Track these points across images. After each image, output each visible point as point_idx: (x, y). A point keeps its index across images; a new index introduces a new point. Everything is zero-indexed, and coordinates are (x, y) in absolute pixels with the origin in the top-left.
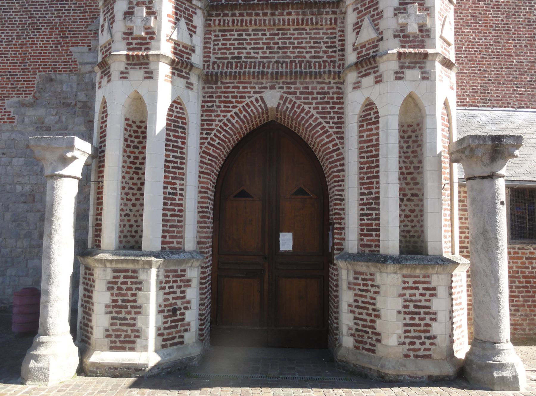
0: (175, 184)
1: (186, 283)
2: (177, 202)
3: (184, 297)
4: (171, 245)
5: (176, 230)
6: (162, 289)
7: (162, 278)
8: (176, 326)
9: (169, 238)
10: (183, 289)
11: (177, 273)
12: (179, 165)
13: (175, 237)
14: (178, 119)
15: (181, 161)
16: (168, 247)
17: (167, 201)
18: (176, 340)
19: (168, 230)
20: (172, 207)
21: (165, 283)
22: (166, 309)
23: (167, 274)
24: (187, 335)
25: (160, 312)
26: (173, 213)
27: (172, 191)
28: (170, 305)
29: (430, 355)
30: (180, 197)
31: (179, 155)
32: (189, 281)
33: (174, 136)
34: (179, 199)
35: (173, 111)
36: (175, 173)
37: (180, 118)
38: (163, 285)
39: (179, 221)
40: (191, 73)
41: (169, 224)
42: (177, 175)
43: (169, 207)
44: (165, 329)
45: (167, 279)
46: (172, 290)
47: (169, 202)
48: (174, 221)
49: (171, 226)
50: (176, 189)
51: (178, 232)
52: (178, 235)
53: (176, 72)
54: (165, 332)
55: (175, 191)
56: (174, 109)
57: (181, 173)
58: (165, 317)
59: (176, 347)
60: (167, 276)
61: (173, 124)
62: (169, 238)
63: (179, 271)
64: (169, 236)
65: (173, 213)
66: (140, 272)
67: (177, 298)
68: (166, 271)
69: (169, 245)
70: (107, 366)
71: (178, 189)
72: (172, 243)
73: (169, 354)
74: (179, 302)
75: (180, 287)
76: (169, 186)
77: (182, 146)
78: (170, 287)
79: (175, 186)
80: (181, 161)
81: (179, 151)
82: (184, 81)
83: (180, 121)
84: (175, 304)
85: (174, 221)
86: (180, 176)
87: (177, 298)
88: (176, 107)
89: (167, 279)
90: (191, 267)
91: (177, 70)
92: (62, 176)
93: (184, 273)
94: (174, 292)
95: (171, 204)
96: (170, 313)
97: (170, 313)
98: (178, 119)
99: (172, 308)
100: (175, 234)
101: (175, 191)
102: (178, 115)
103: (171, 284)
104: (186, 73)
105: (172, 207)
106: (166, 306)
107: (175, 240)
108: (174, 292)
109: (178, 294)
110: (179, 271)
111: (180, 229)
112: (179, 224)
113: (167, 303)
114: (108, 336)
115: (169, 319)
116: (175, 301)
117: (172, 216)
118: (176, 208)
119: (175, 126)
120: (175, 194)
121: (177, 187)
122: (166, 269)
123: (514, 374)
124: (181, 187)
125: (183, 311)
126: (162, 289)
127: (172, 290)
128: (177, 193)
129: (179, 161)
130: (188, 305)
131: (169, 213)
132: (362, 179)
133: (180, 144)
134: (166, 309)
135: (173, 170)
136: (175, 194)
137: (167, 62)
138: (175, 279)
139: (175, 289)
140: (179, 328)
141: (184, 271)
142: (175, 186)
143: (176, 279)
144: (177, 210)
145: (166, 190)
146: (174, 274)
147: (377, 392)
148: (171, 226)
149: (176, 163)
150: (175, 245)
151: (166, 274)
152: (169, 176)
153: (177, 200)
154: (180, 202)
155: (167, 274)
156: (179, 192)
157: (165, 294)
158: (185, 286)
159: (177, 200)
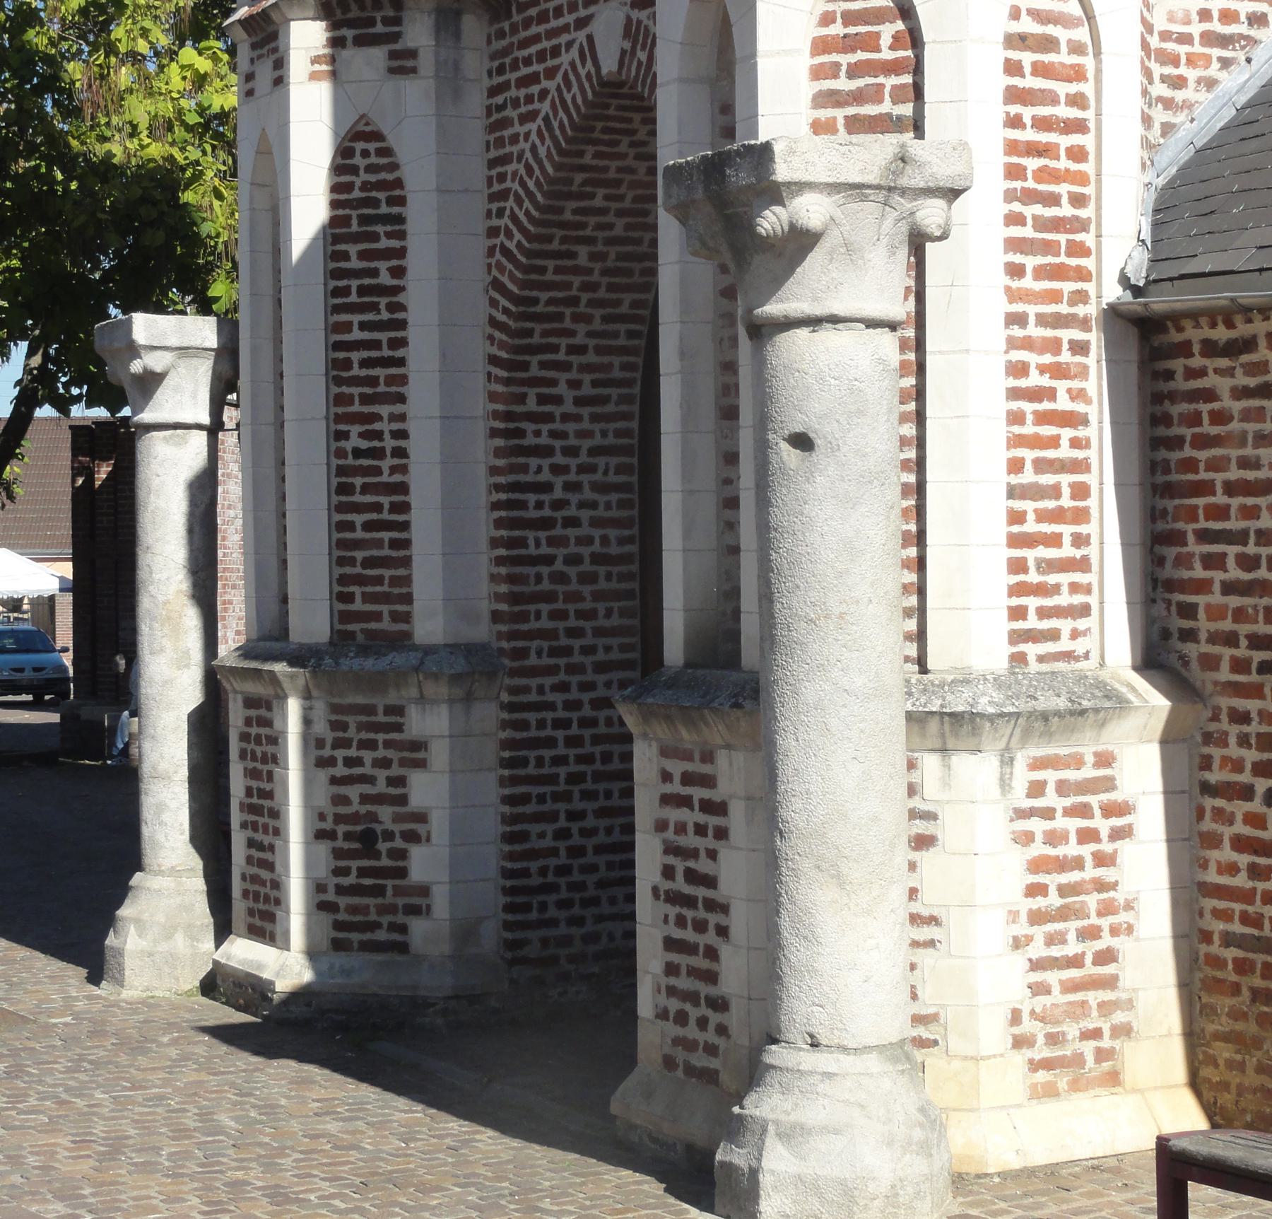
0: (377, 417)
1: (406, 754)
2: (385, 478)
3: (403, 800)
4: (373, 626)
5: (387, 573)
6: (323, 763)
7: (321, 728)
8: (379, 891)
9: (364, 602)
10: (396, 771)
11: (373, 719)
12: (386, 352)
13: (386, 598)
14: (374, 194)
15: (393, 334)
16: (362, 631)
17: (350, 480)
18: (381, 935)
19: (359, 575)
20: (369, 499)
21: (334, 747)
22: (341, 829)
23: (340, 717)
24: (418, 928)
25: (320, 835)
26: (374, 516)
27: (364, 444)
28: (355, 818)
29: (716, 1072)
30: (396, 461)
31: (385, 315)
32: (418, 745)
33: (363, 255)
34: (393, 470)
35: (354, 170)
36: (373, 381)
37: (382, 185)
38: (327, 752)
39: (395, 544)
40: (406, 15)
41: (359, 555)
42: (382, 388)
43: (358, 498)
44: (340, 890)
45: (340, 734)
46: (357, 771)
47: (358, 481)
48: (379, 544)
49: (369, 563)
50: (378, 435)
51: (395, 581)
52: (396, 591)
53: (349, 33)
54: (343, 901)
55: (376, 444)
56: (358, 160)
57: (394, 376)
58: (338, 854)
59: (379, 957)
60: (336, 726)
61: (354, 213)
62: (364, 602)
63: (381, 710)
64: (363, 594)
65: (374, 516)
66: (413, 713)
67: (379, 799)
68: (335, 709)
69: (365, 626)
70: (233, 976)
71: (387, 436)
72: (377, 616)
73: (346, 972)
74: (385, 813)
75: (385, 763)
76: (355, 429)
77: (395, 282)
78: (349, 762)
79: (377, 426)
80: (393, 334)
81: (383, 301)
82: (378, 54)
83: (382, 196)
84: (373, 817)
85: (379, 544)
86: (393, 389)
87: (379, 799)
88: (365, 154)
89: (340, 734)
90: (422, 700)
91: (351, 24)
92: (790, 324)
93: (399, 719)
94: (370, 780)
95: (366, 489)
96: (355, 845)
97: (355, 845)
98: (374, 194)
99: (359, 828)
100: (385, 588)
101: (376, 444)
102: (372, 178)
103: (353, 752)
104: (387, 21)
105: (369, 499)
106: (339, 819)
107: (385, 609)
108: (370, 780)
109: (381, 787)
110: (381, 710)
111: (401, 572)
112: (394, 554)
113: (342, 810)
114: (1020, 1042)
115: (354, 864)
116: (369, 807)
117: (368, 526)
118: (385, 500)
119: (364, 220)
120: (378, 453)
121: (384, 426)
122: (336, 700)
123: (754, 1164)
124: (395, 426)
125: (399, 843)
126: (323, 763)
127: (357, 771)
128: (383, 449)
129: (383, 336)
130: (420, 828)
132: (1019, 369)
133: (385, 279)
134: (341, 829)
135: (364, 372)
136: (378, 453)
137: (311, 14)
138: (365, 735)
139: (367, 769)
140: (389, 898)
141: (399, 710)
142: (377, 426)
143: (372, 736)
144: (387, 506)
145: (342, 444)
146: (364, 718)
147: (307, 1082)
148: (369, 563)
149: (376, 345)
150: (386, 625)
151: (334, 717)
152: (351, 396)
153: (386, 472)
154: (397, 478)
155: (340, 717)
156: (389, 443)
157: (334, 781)
158: (403, 763)
159: (386, 472)
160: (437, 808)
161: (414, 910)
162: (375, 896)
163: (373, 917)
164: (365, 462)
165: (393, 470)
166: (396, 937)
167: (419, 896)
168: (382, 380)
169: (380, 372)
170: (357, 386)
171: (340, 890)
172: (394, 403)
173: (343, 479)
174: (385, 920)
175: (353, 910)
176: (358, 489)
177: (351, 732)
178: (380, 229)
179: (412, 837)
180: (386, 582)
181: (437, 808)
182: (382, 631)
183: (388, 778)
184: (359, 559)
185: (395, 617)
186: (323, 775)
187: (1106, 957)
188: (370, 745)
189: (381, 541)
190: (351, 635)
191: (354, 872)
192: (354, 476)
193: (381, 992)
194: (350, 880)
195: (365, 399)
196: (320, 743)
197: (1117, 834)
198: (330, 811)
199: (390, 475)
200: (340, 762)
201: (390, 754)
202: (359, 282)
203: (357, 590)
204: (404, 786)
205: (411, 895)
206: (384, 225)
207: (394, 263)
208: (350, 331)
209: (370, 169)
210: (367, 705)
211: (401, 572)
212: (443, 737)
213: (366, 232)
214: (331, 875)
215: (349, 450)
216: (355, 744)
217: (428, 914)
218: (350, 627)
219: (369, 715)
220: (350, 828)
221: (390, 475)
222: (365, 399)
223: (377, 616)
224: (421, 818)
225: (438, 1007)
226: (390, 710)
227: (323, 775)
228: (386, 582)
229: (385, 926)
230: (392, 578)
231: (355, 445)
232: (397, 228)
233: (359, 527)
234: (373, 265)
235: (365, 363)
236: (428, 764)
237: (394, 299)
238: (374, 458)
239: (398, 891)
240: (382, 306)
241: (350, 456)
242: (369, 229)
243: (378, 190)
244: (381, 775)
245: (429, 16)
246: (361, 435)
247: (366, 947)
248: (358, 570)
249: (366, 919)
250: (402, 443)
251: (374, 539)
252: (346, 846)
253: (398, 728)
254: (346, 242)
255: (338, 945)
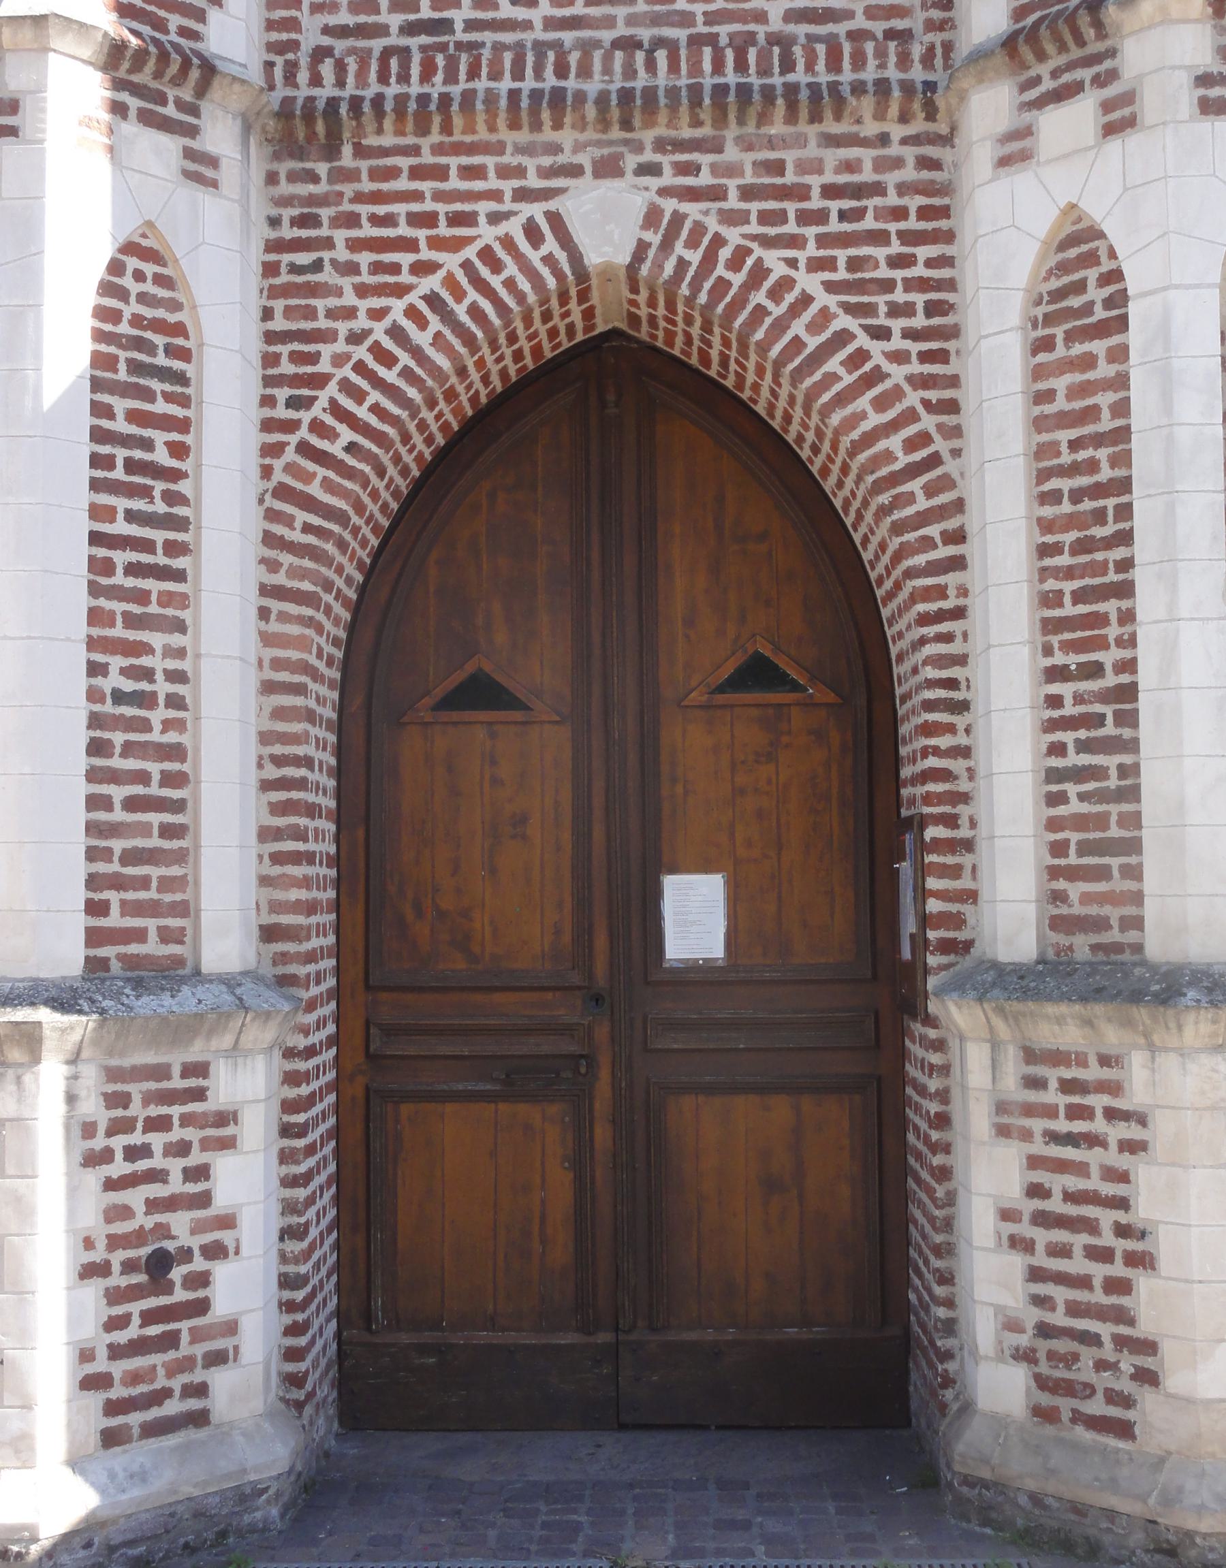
0: (147, 649)
2: (155, 736)
4: (134, 949)
5: (154, 872)
7: (92, 1107)
8: (171, 1340)
10: (196, 1158)
11: (165, 1085)
12: (161, 559)
14: (148, 335)
16: (121, 958)
17: (106, 735)
18: (172, 1407)
19: (117, 875)
20: (132, 764)
21: (110, 1133)
23: (119, 1087)
24: (221, 1381)
26: (138, 790)
27: (128, 686)
28: (139, 1237)
30: (172, 714)
31: (160, 507)
33: (134, 416)
34: (167, 725)
35: (122, 294)
36: (142, 597)
38: (99, 1143)
39: (168, 831)
41: (118, 845)
42: (154, 609)
43: (117, 762)
45: (119, 1113)
46: (142, 1165)
47: (118, 738)
48: (145, 830)
49: (130, 857)
50: (147, 674)
51: (167, 884)
52: (168, 898)
53: (134, 103)
54: (119, 1368)
55: (144, 686)
56: (127, 281)
57: (170, 594)
58: (115, 1296)
60: (117, 1100)
61: (123, 355)
63: (176, 1071)
64: (123, 903)
65: (138, 790)
67: (171, 1204)
68: (114, 1075)
69: (122, 949)
71: (159, 676)
72: (139, 935)
73: (141, 1476)
74: (180, 1222)
75: (182, 1149)
76: (116, 662)
78: (132, 1153)
79: (145, 661)
81: (159, 487)
83: (159, 340)
84: (163, 1231)
85: (145, 830)
86: (170, 612)
87: (171, 1204)
88: (139, 276)
89: (119, 1113)
91: (137, 90)
93: (201, 1082)
95: (129, 749)
97: (141, 1278)
98: (148, 335)
100: (152, 894)
101: (144, 686)
103: (136, 1138)
104: (181, 105)
105: (132, 764)
106: (115, 1242)
107: (151, 924)
109: (176, 1185)
111: (175, 871)
112: (167, 844)
115: (135, 1308)
117: (132, 804)
118: (154, 768)
120: (146, 700)
122: (114, 1062)
124: (172, 664)
125: (199, 1264)
126: (93, 1160)
127: (142, 1165)
128: (154, 694)
129: (159, 536)
130: (226, 1237)
131: (118, 793)
133: (161, 456)
135: (130, 582)
136: (146, 700)
139: (157, 1161)
141: (199, 1069)
142: (145, 661)
143: (164, 1110)
145: (99, 681)
146: (152, 1085)
149: (147, 546)
150: (152, 947)
151: (111, 1088)
153: (157, 727)
154: (172, 737)
155: (119, 1087)
156: (162, 687)
157: (111, 1185)
158: (206, 1145)
159: (157, 727)
160: (249, 1204)
161: (217, 1359)
162: (164, 1350)
163: (161, 1382)
164: (128, 711)
165: (167, 725)
166: (193, 1404)
167: (223, 1336)
168: (154, 598)
169: (152, 585)
170: (121, 600)
171: (116, 1352)
172: (171, 632)
173: (98, 734)
174: (176, 1384)
175: (134, 1378)
176: (118, 750)
177: (136, 1109)
178: (156, 385)
179: (216, 1251)
180: (154, 884)
181: (249, 1204)
182: (147, 956)
183: (185, 1171)
184: (117, 853)
185: (167, 936)
186: (93, 1178)
187: (1119, 1286)
188: (159, 1124)
189: (148, 825)
190: (103, 964)
191: (136, 1320)
192: (114, 729)
193: (196, 1492)
194: (133, 1331)
195: (132, 621)
196: (89, 1130)
197: (1132, 1147)
198: (100, 1232)
199: (163, 732)
200: (119, 1156)
201: (191, 1134)
202: (127, 453)
203: (113, 897)
204: (207, 1178)
205: (212, 1338)
206: (162, 381)
207: (175, 436)
208: (112, 520)
209: (143, 298)
210: (158, 1066)
211: (175, 871)
212: (258, 1101)
213: (137, 384)
214: (101, 1330)
215: (108, 691)
216: (140, 1125)
217: (235, 1360)
218: (103, 952)
219: (159, 1080)
220: (131, 1253)
221: (163, 732)
222: (132, 621)
223: (139, 935)
224: (227, 1222)
225: (271, 1492)
226: (190, 1070)
227: (93, 1178)
228: (154, 884)
229: (177, 1393)
230: (162, 879)
231: (116, 685)
232: (179, 389)
233: (117, 806)
234: (147, 433)
235: (133, 570)
236: (238, 1143)
237: (173, 487)
238: (140, 706)
239: (197, 1336)
240: (157, 493)
241: (109, 700)
242: (142, 381)
243: (155, 331)
244: (175, 1166)
245: (234, 119)
246: (124, 672)
247: (153, 1430)
248: (115, 867)
249: (151, 1387)
250: (180, 689)
251: (140, 823)
252: (124, 1281)
253: (199, 1095)
254: (112, 393)
255: (110, 1439)
